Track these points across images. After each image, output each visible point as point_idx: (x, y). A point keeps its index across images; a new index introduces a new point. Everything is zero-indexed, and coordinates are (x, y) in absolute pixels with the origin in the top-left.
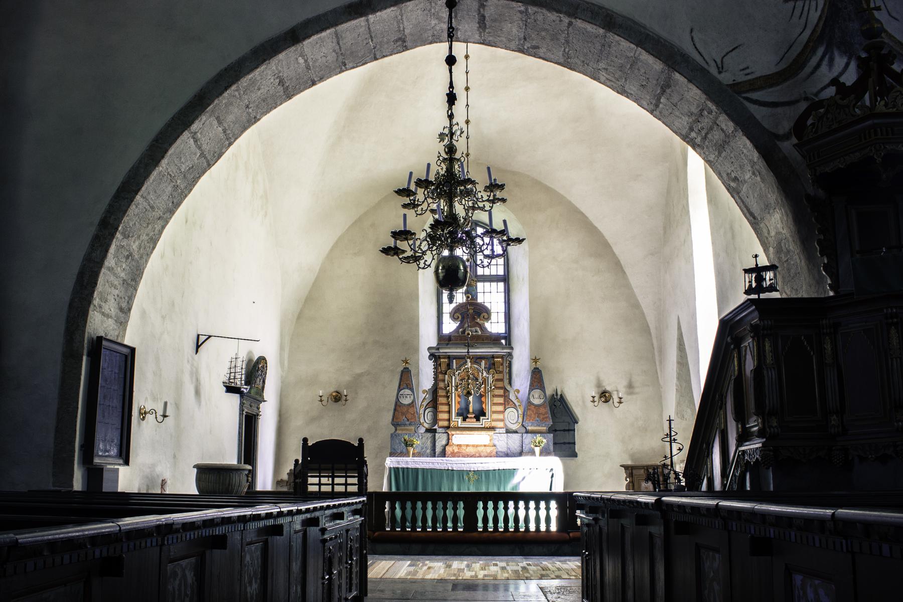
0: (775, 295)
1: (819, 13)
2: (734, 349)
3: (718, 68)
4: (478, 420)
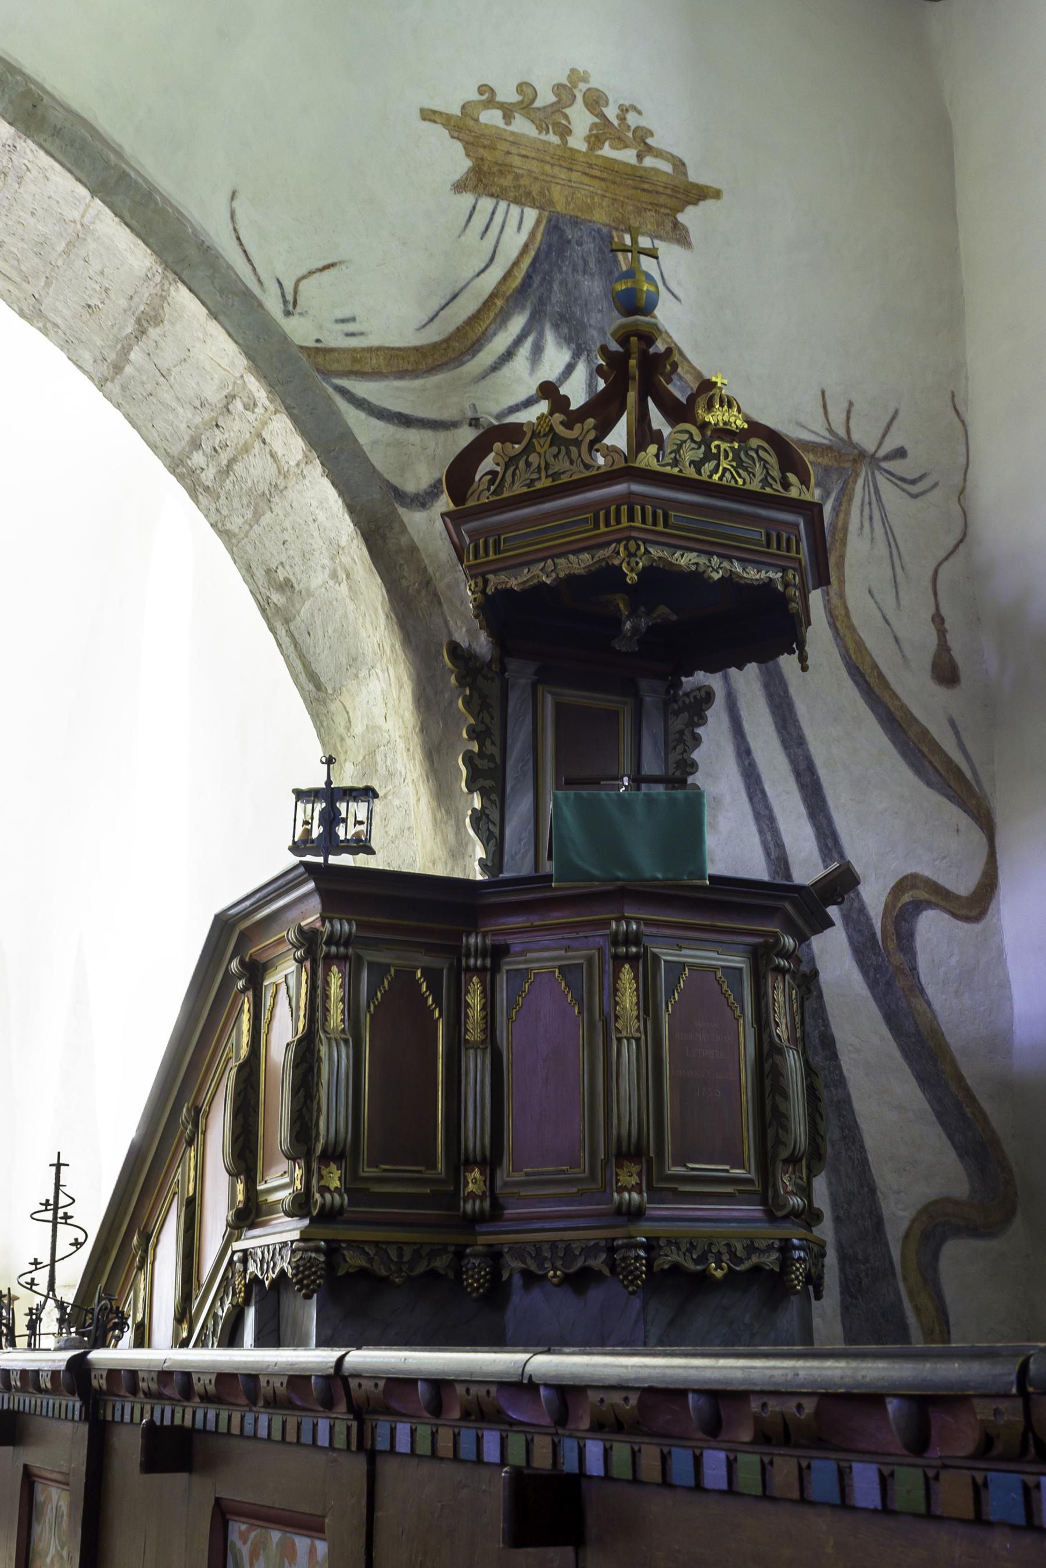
0: (360, 861)
1: (523, 237)
2: (243, 991)
3: (285, 302)
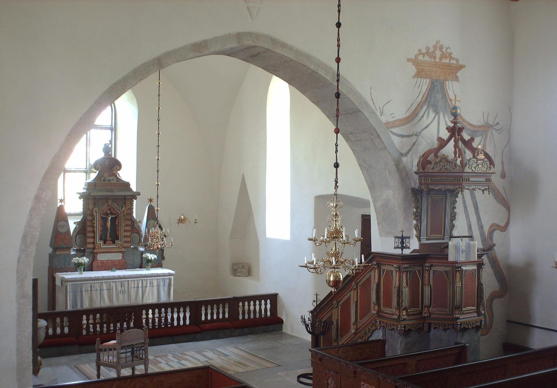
4: (114, 243)
